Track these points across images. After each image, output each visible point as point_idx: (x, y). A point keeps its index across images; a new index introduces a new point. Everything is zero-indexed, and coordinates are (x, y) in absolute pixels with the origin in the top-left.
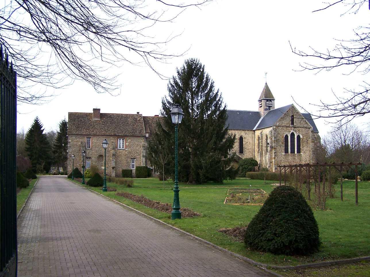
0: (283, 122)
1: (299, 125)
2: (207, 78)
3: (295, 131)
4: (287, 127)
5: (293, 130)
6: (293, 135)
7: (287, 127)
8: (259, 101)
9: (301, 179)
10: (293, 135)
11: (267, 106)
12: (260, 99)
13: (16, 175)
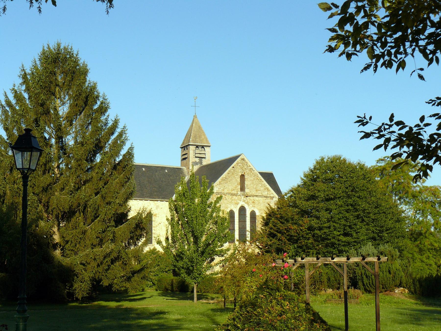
0: (226, 185)
1: (254, 193)
2: (120, 135)
3: (247, 203)
4: (233, 195)
5: (244, 201)
6: (242, 210)
7: (233, 195)
8: (181, 148)
9: (39, 176)
10: (242, 210)
11: (196, 157)
12: (182, 145)
13: (248, 239)
